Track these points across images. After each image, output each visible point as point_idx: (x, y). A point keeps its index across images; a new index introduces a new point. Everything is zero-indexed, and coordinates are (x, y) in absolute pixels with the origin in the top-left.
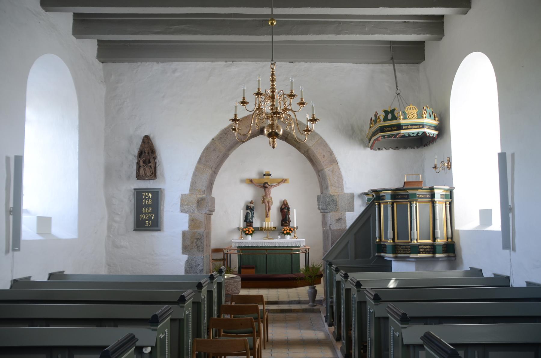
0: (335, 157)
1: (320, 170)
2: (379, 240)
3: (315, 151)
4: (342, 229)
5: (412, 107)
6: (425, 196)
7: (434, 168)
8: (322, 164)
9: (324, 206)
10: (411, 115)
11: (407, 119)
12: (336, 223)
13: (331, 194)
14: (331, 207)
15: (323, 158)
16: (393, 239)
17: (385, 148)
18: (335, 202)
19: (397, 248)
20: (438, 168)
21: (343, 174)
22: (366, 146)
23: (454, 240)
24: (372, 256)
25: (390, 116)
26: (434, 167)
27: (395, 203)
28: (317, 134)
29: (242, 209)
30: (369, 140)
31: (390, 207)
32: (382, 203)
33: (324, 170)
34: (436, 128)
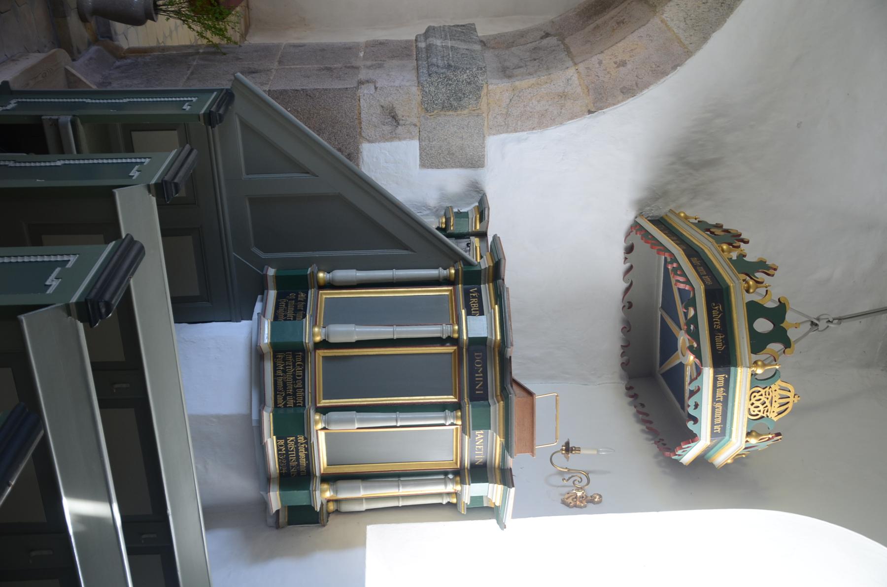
0: (614, 104)
1: (567, 41)
2: (322, 282)
3: (642, 31)
4: (361, 128)
5: (788, 403)
6: (479, 450)
7: (567, 444)
8: (595, 59)
9: (440, 63)
10: (763, 398)
11: (751, 389)
12: (382, 107)
13: (485, 91)
14: (437, 88)
15: (615, 63)
16: (325, 344)
17: (631, 267)
18: (455, 104)
19: (294, 357)
20: (568, 458)
21: (554, 133)
22: (642, 207)
23: (333, 521)
24: (263, 255)
25: (763, 325)
26: (571, 446)
27: (455, 348)
28: (705, 39)
29: (272, 412)
30: (662, 218)
31: (442, 332)
32: (455, 293)
33: (571, 62)
34: (702, 461)
